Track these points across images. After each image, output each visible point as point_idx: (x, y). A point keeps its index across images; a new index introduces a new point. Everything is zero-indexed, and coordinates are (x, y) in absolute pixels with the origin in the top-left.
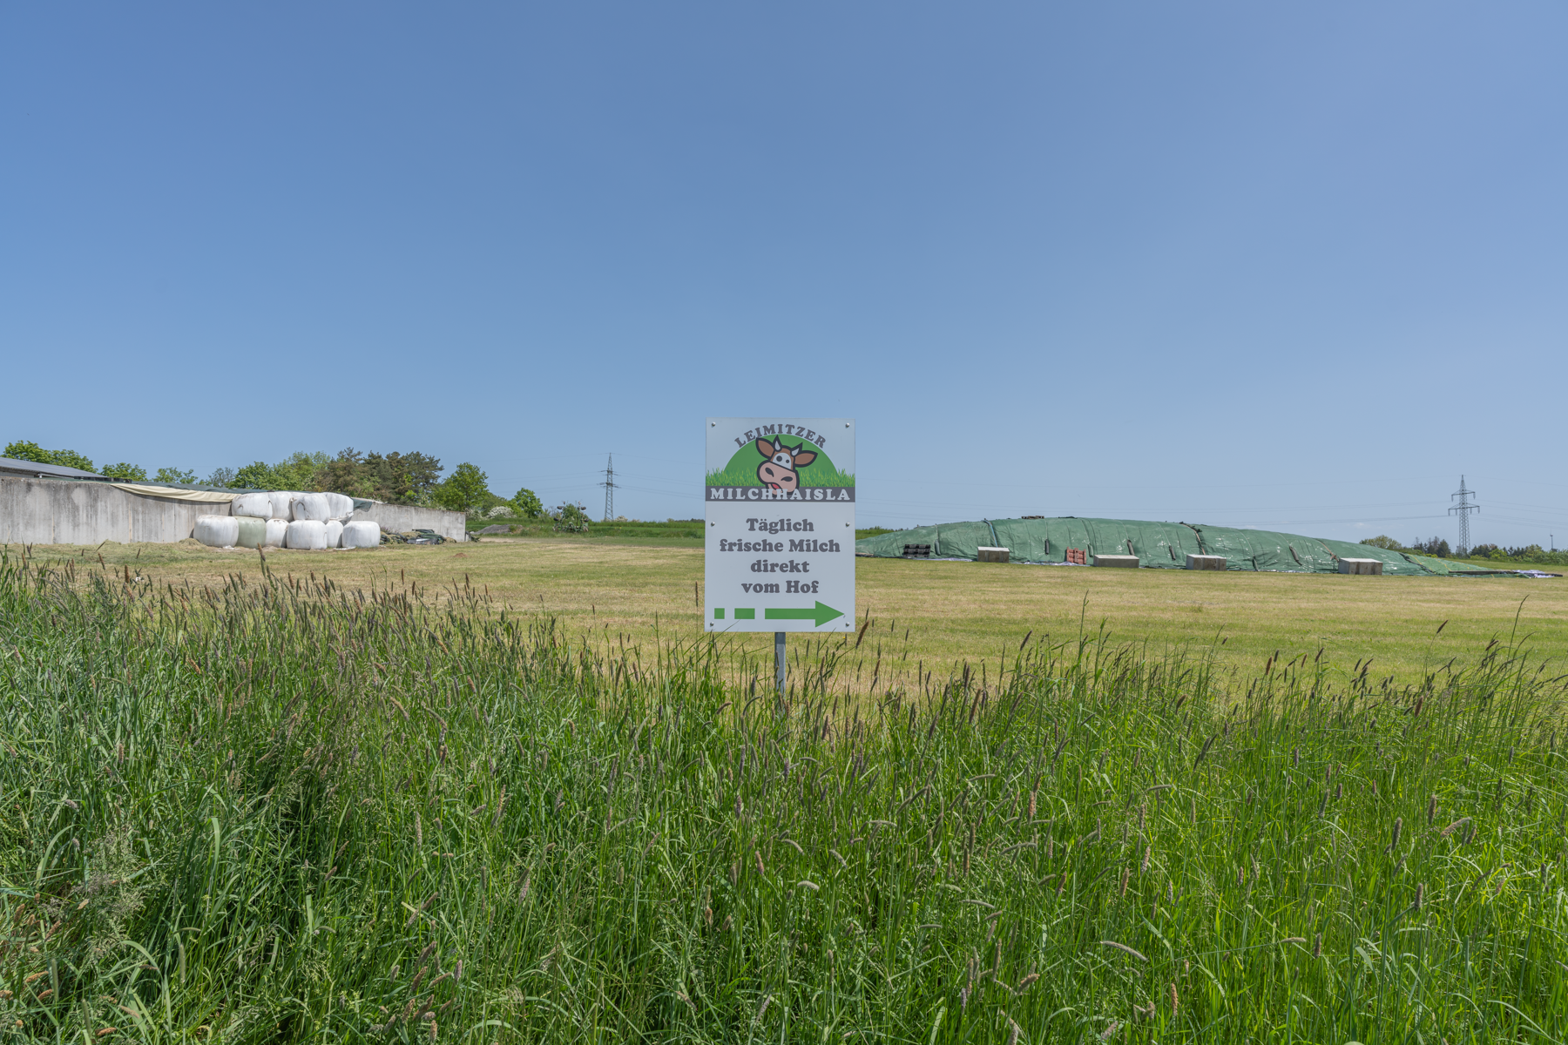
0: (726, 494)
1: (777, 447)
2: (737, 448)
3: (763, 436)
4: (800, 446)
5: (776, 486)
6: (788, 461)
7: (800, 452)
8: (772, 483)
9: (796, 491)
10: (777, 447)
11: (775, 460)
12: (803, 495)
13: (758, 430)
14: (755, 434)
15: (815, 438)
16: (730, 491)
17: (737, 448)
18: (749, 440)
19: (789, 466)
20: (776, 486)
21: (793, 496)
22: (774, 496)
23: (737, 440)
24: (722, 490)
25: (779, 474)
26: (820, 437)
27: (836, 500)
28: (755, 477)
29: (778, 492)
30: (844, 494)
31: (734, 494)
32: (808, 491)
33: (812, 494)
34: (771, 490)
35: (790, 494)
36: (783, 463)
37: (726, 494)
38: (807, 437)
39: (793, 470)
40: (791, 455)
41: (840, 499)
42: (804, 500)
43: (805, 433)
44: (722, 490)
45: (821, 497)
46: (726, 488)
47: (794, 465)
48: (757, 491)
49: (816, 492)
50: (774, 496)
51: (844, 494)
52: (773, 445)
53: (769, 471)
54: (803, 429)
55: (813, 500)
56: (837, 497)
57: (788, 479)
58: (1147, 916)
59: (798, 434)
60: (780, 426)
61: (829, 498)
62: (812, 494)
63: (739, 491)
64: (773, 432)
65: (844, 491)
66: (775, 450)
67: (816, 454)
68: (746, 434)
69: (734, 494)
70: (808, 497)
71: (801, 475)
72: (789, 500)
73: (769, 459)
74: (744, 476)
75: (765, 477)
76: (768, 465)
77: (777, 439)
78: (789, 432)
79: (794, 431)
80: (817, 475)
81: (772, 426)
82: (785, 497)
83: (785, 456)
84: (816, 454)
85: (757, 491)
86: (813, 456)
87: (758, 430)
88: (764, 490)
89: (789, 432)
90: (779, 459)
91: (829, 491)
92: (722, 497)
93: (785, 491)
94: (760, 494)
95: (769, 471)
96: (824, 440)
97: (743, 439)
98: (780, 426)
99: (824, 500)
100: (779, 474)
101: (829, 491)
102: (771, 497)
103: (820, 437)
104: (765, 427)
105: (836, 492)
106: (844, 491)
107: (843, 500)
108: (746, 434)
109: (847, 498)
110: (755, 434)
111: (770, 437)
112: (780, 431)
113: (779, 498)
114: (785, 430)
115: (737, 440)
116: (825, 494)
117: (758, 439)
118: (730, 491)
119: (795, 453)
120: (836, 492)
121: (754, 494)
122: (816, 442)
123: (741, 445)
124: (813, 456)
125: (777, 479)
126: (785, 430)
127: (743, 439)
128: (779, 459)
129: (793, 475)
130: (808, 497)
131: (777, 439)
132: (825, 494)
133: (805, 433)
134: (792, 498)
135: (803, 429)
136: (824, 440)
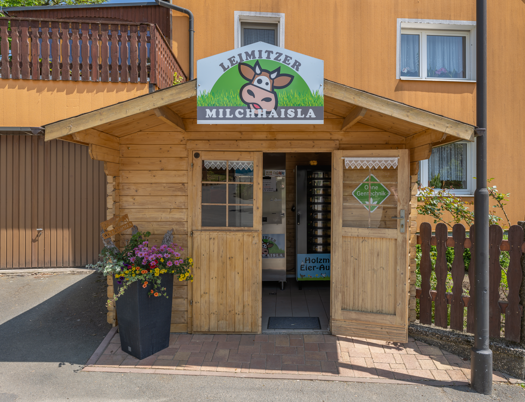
0: (218, 113)
1: (258, 71)
2: (221, 72)
3: (245, 61)
4: (278, 70)
5: (257, 106)
6: (267, 84)
7: (279, 75)
8: (253, 104)
9: (273, 111)
10: (258, 71)
11: (255, 83)
12: (279, 114)
13: (240, 55)
14: (237, 59)
15: (292, 62)
16: (221, 111)
17: (221, 72)
18: (232, 64)
19: (269, 88)
20: (257, 106)
21: (271, 114)
22: (256, 115)
23: (222, 65)
24: (214, 111)
25: (259, 96)
26: (296, 62)
27: (279, 257)
28: (238, 98)
29: (259, 112)
30: (281, 255)
31: (224, 113)
32: (271, 255)
33: (272, 255)
34: (253, 110)
35: (266, 255)
36: (263, 85)
37: (218, 113)
38: (284, 62)
39: (273, 92)
40: (270, 78)
41: (308, 116)
42: (270, 257)
43: (282, 58)
44: (214, 111)
45: (275, 256)
46: (218, 108)
47: (273, 87)
48: (242, 111)
49: (274, 255)
50: (256, 115)
51: (281, 255)
52: (254, 69)
53: (250, 93)
54: (280, 54)
55: (272, 257)
56: (306, 115)
57: (268, 100)
58: (425, 206)
59: (276, 59)
60: (260, 52)
61: (277, 256)
62: (272, 255)
63: (228, 111)
64: (254, 57)
65: (281, 254)
66: (256, 74)
67: (292, 77)
68: (230, 59)
69: (224, 113)
70: (271, 256)
71: (279, 96)
72: (266, 257)
73: (251, 82)
74: (228, 97)
75: (248, 98)
76: (250, 87)
77: (257, 63)
78: (268, 57)
79: (273, 57)
80: (293, 96)
81: (253, 52)
82: (265, 256)
83: (265, 79)
84: (292, 77)
85: (242, 111)
86: (290, 78)
87: (240, 55)
88: (248, 110)
89: (268, 57)
90: (260, 81)
91: (277, 254)
92: (214, 116)
93: (265, 255)
94: (245, 113)
95: (250, 93)
96: (300, 65)
97: (227, 64)
98: (260, 52)
99: (276, 257)
100: (259, 96)
101: (277, 254)
102: (253, 116)
103: (296, 62)
104: (247, 53)
105: (279, 255)
106: (281, 254)
107: (281, 257)
108: (230, 59)
109: (282, 256)
110: (237, 59)
111: (251, 61)
112: (260, 56)
113: (259, 116)
114: (264, 56)
115: (222, 65)
116: (276, 255)
117: (240, 64)
118: (221, 111)
119: (273, 76)
120: (279, 255)
121: (240, 113)
122: (293, 66)
123: (225, 69)
124: (290, 78)
125: (258, 99)
126: (264, 56)
127: (227, 64)
128: (260, 81)
129: (272, 96)
130: (271, 256)
131: (257, 63)
132: (276, 255)
133: (282, 58)
134: (270, 116)
135: (280, 54)
136: (300, 65)
